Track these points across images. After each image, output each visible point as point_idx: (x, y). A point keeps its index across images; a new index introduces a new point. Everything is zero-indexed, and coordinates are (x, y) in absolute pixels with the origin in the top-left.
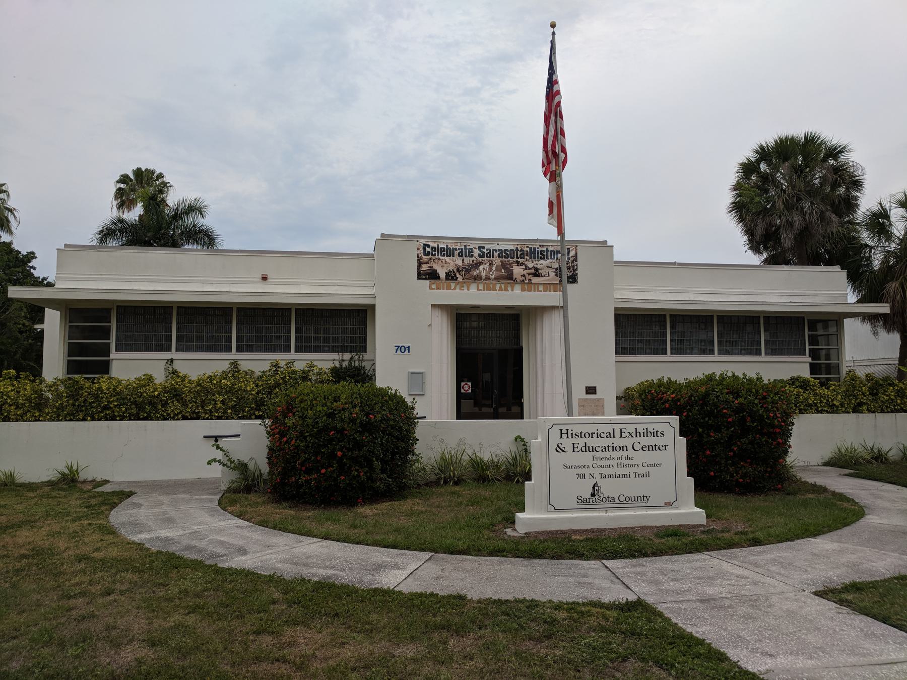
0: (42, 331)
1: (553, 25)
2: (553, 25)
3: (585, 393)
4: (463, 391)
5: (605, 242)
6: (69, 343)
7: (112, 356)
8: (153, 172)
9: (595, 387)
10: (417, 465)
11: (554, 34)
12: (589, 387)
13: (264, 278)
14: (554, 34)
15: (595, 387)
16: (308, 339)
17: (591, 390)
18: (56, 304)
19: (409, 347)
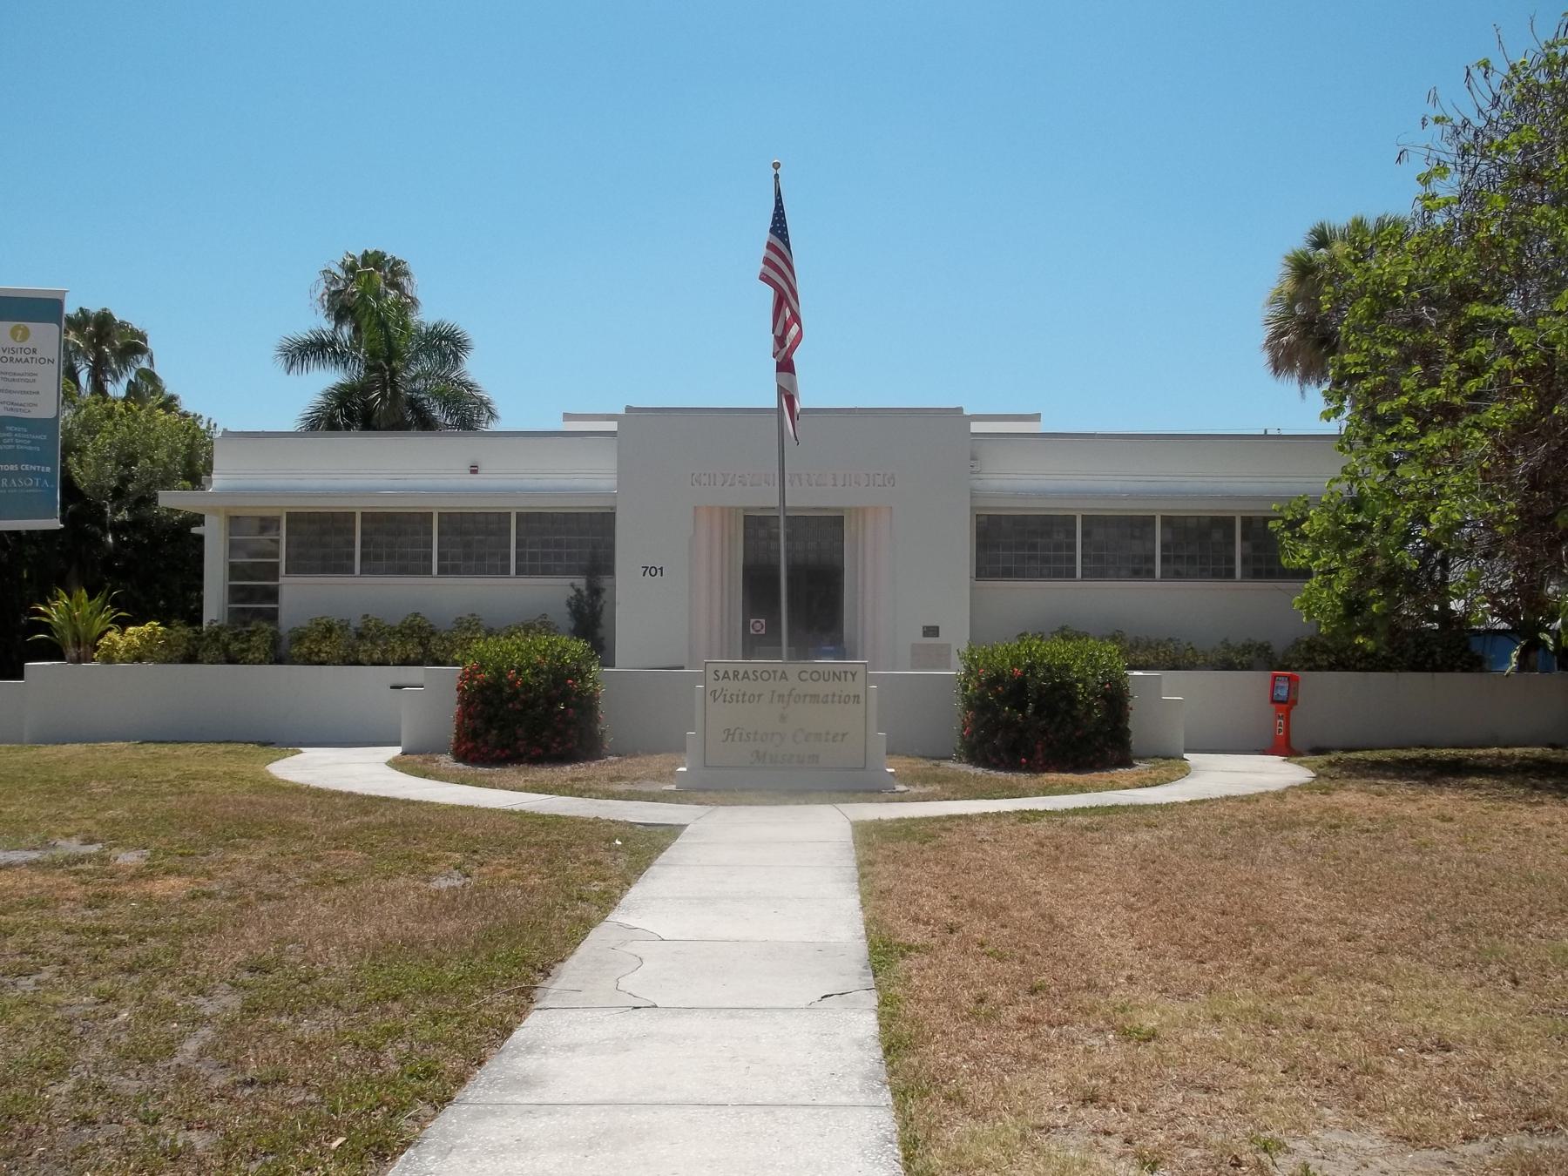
0: (201, 538)
1: (777, 166)
2: (777, 166)
3: (921, 633)
4: (752, 631)
5: (960, 409)
6: (230, 586)
7: (282, 580)
8: (383, 255)
9: (938, 627)
10: (131, 487)
11: (777, 176)
12: (927, 627)
13: (474, 469)
14: (777, 176)
15: (938, 627)
16: (533, 557)
17: (931, 631)
18: (215, 511)
19: (661, 569)
